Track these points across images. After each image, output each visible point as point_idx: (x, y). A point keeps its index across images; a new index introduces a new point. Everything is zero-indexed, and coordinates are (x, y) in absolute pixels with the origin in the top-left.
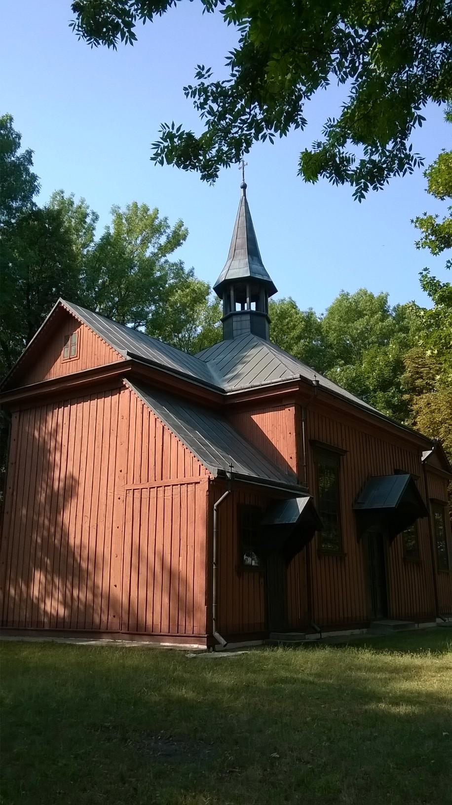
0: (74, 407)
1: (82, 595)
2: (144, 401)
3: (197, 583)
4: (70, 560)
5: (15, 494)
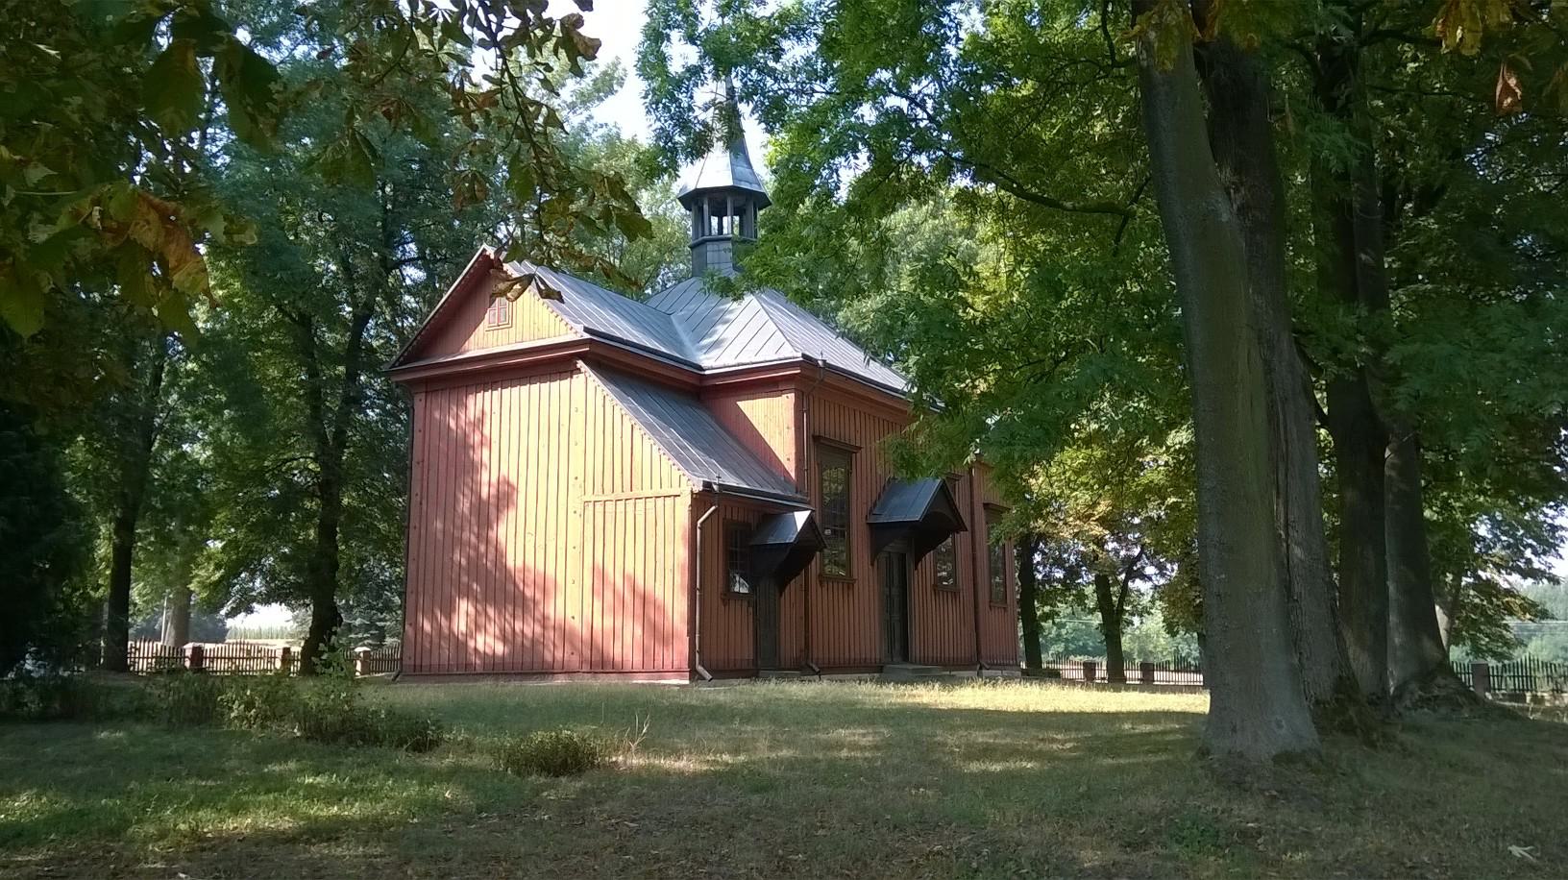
0: (506, 392)
1: (527, 628)
2: (607, 391)
3: (676, 607)
4: (510, 587)
5: (424, 502)
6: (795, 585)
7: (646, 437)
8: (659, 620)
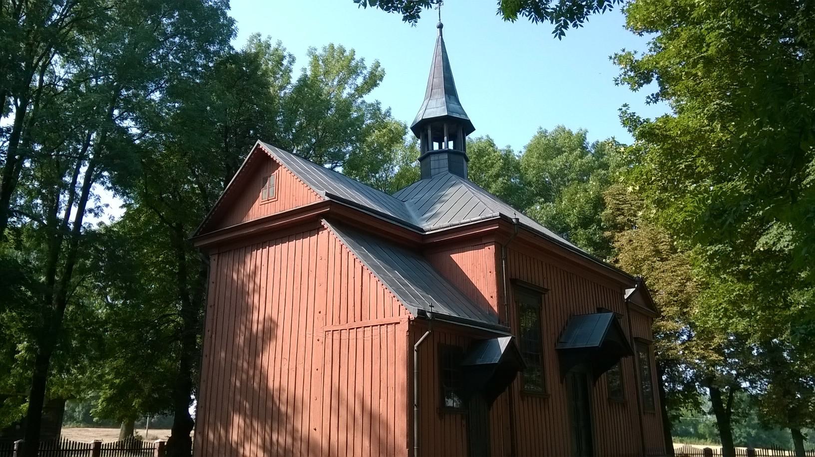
0: (272, 249)
2: (343, 241)
4: (270, 404)
5: (213, 336)
6: (501, 400)
7: (372, 275)
8: (383, 434)
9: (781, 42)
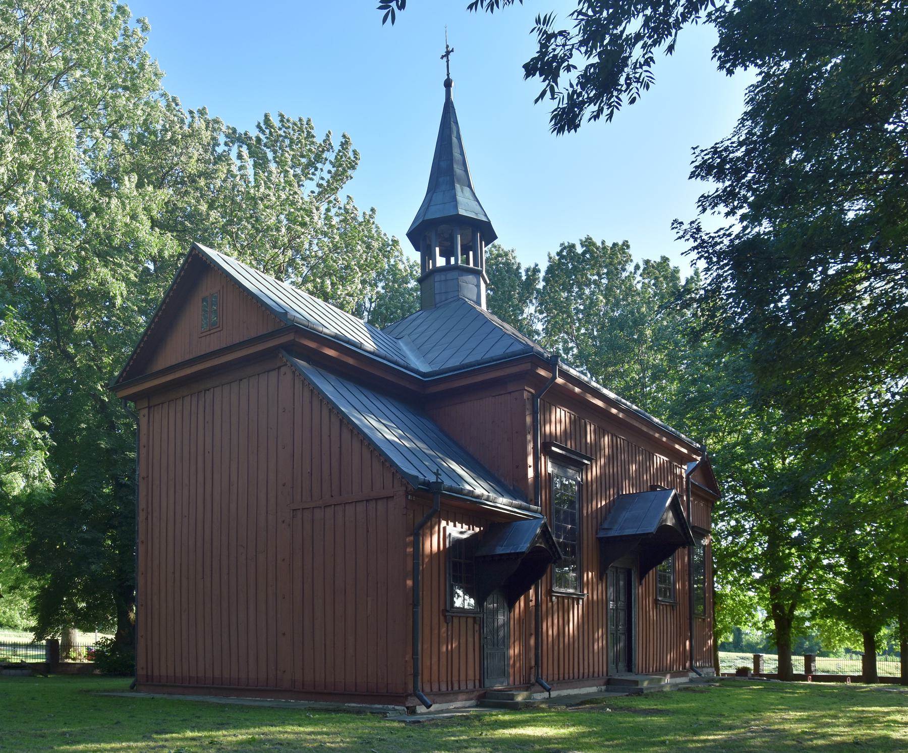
9: (765, 222)
